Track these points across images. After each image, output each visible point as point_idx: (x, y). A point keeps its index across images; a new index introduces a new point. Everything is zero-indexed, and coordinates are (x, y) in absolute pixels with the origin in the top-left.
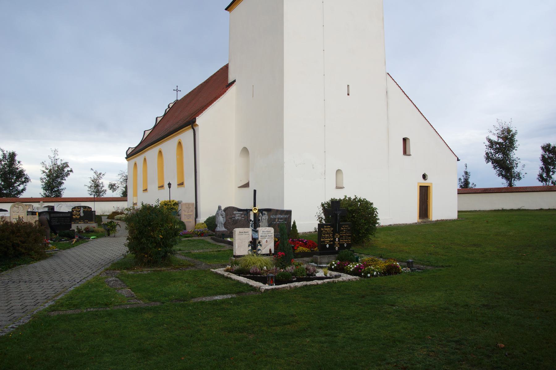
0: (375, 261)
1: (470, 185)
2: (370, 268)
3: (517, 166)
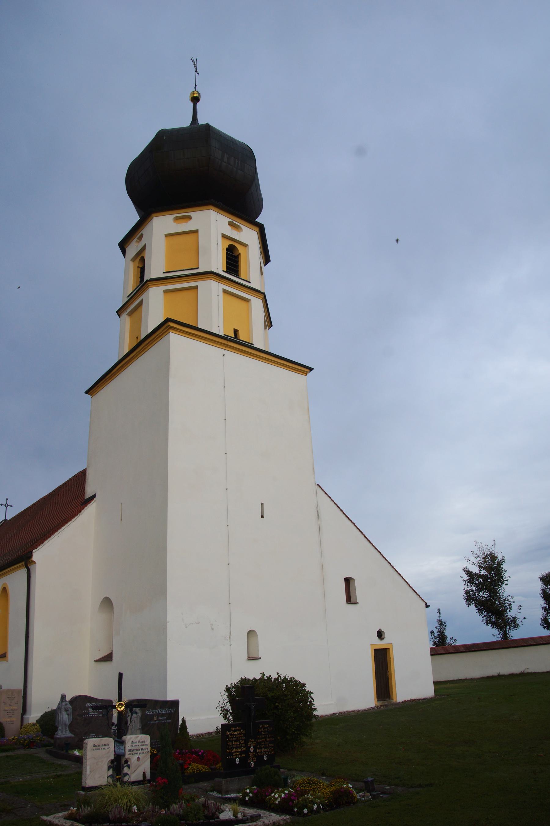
0: (314, 783)
1: (448, 641)
2: (308, 798)
3: (511, 608)
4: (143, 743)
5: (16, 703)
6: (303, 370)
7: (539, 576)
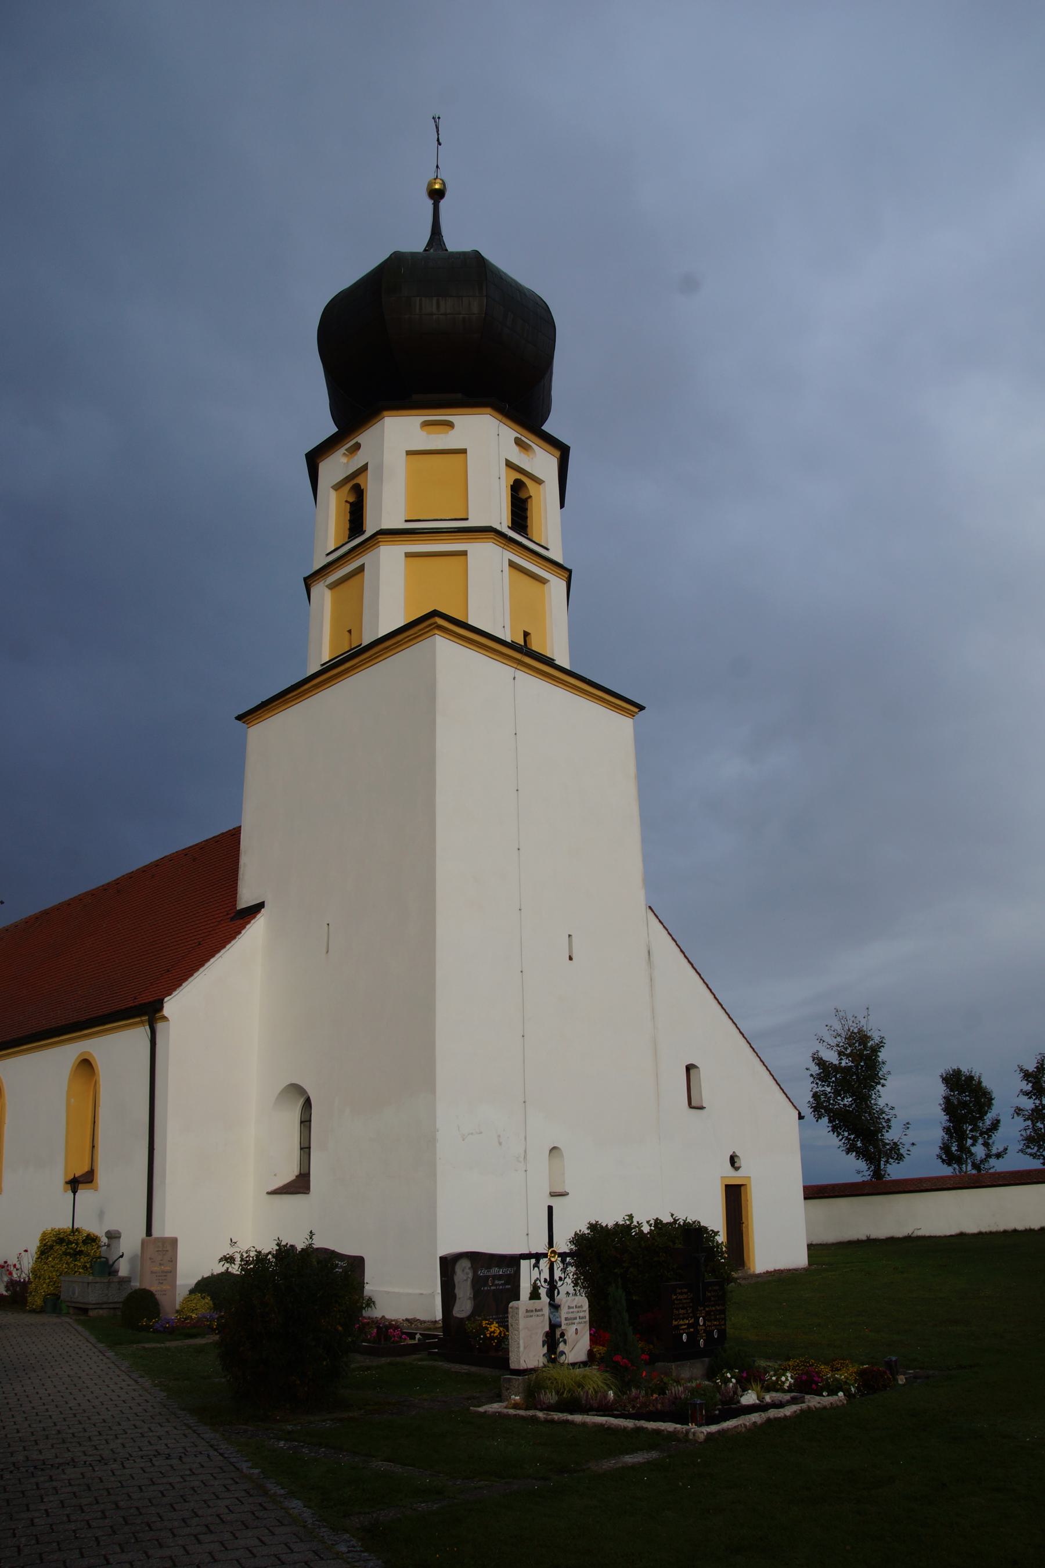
3: (889, 1127)
4: (580, 1309)
5: (169, 1261)
6: (629, 710)
7: (941, 1074)
